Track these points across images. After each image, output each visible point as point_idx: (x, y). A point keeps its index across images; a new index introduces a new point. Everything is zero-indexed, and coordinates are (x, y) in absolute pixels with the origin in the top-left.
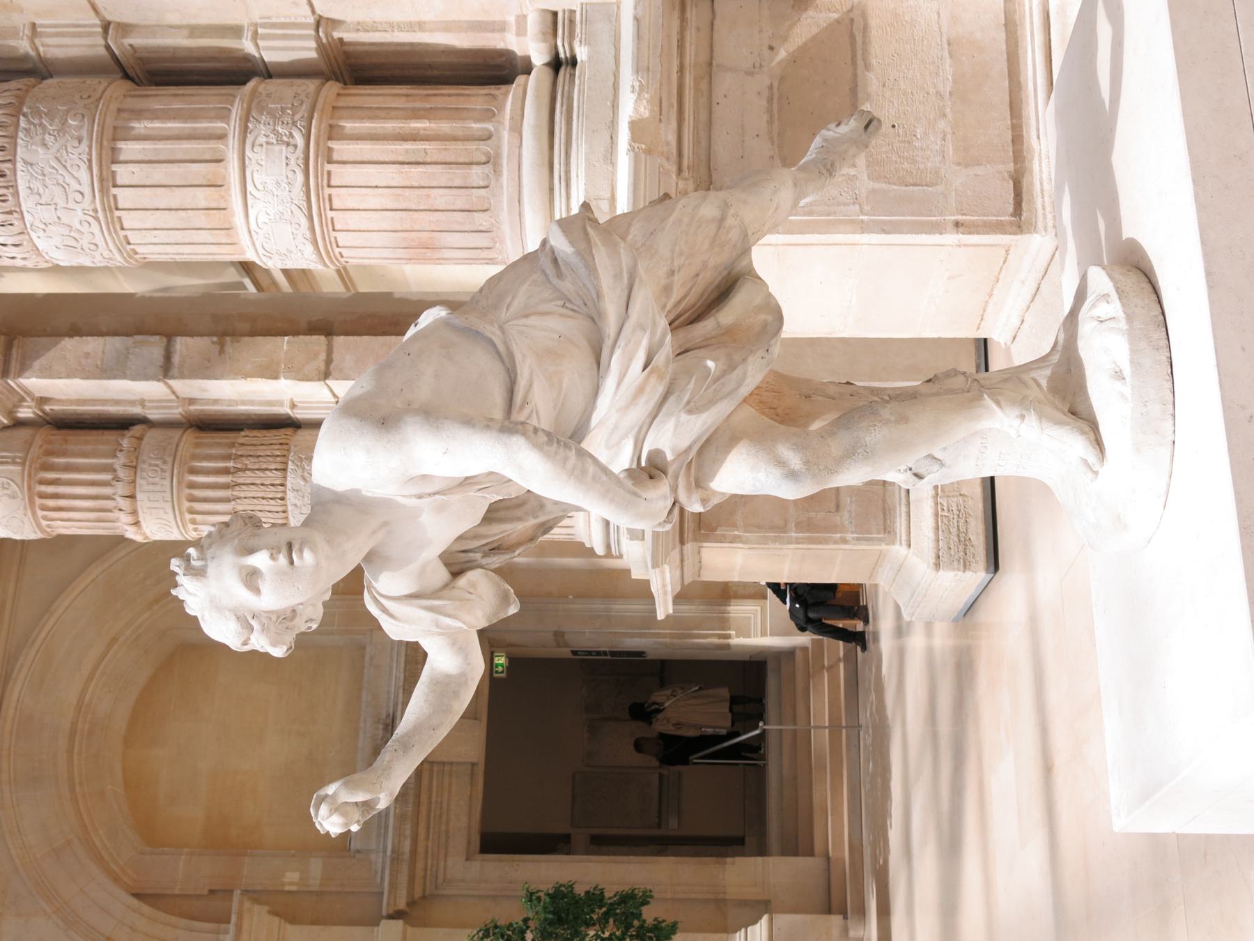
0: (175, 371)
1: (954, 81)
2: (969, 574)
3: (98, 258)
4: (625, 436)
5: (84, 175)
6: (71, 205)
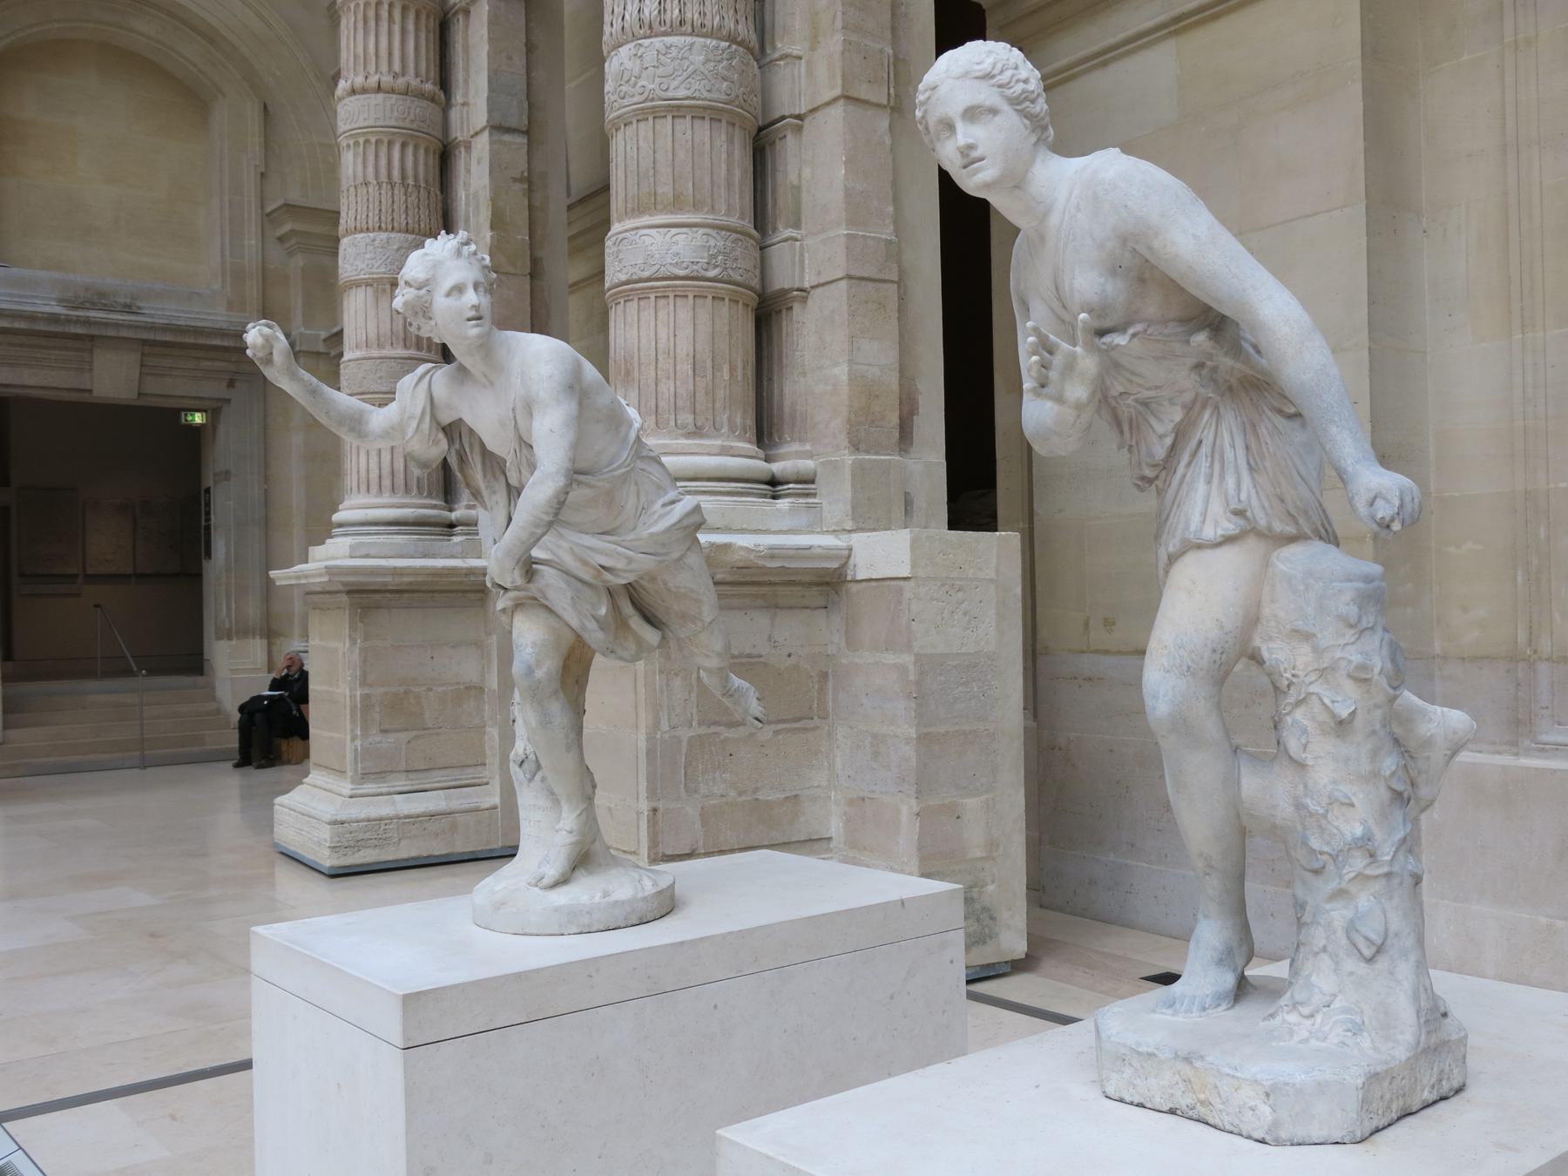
0: (496, 137)
1: (767, 802)
2: (327, 852)
3: (613, 98)
5: (682, 93)
6: (658, 80)
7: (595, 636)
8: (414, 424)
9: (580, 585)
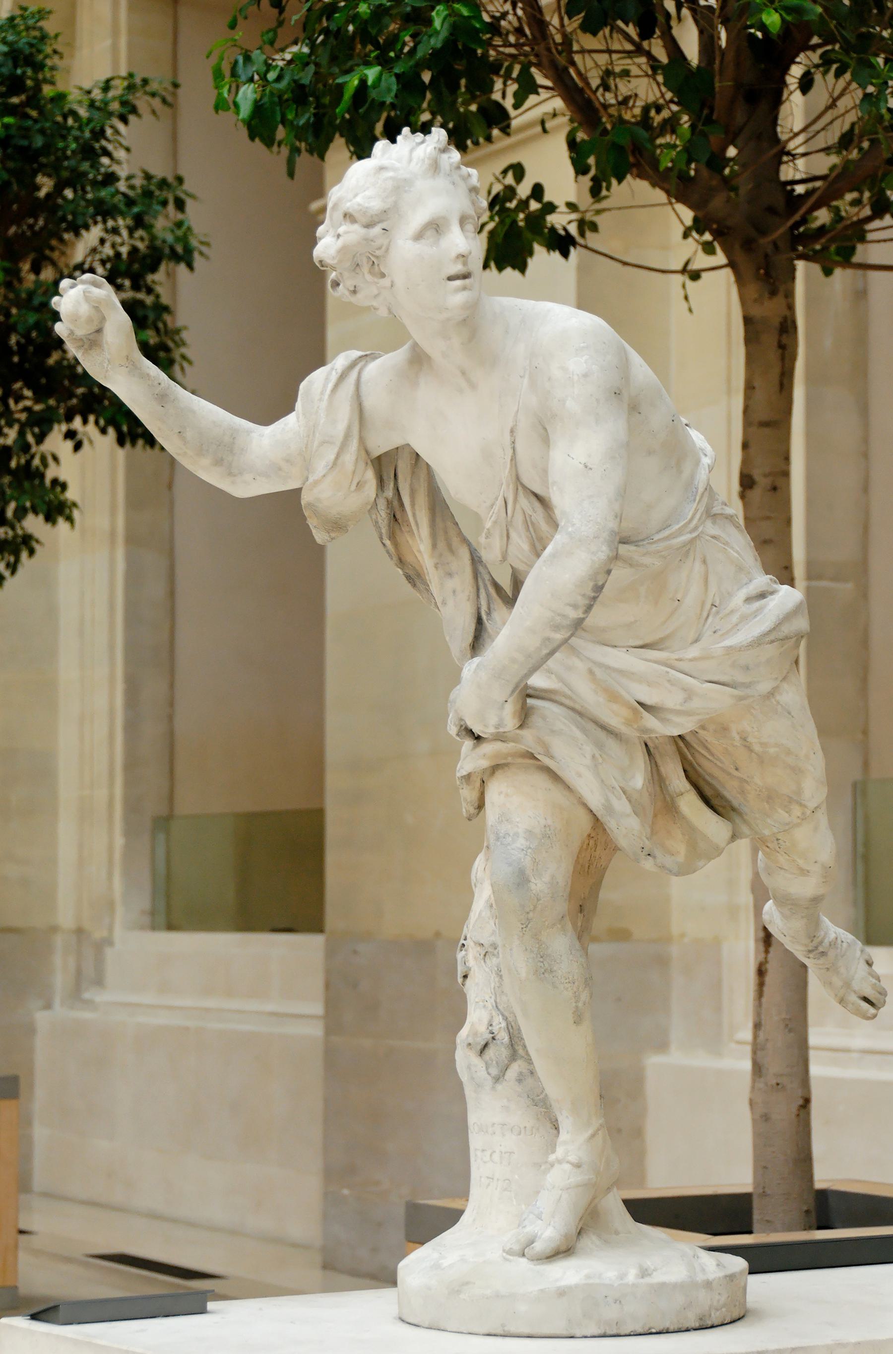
4: (561, 680)
7: (626, 827)
8: (330, 455)
9: (602, 735)
